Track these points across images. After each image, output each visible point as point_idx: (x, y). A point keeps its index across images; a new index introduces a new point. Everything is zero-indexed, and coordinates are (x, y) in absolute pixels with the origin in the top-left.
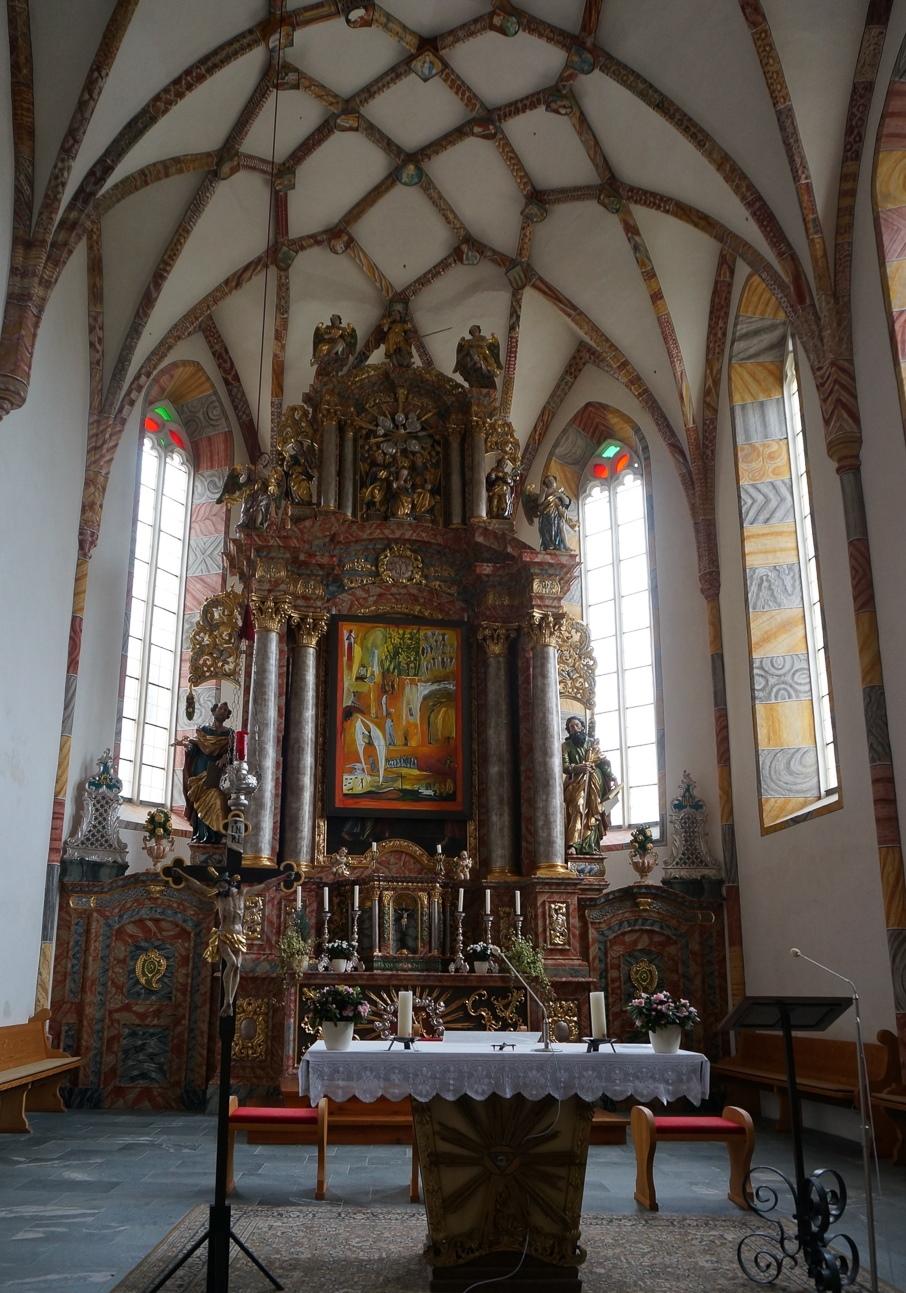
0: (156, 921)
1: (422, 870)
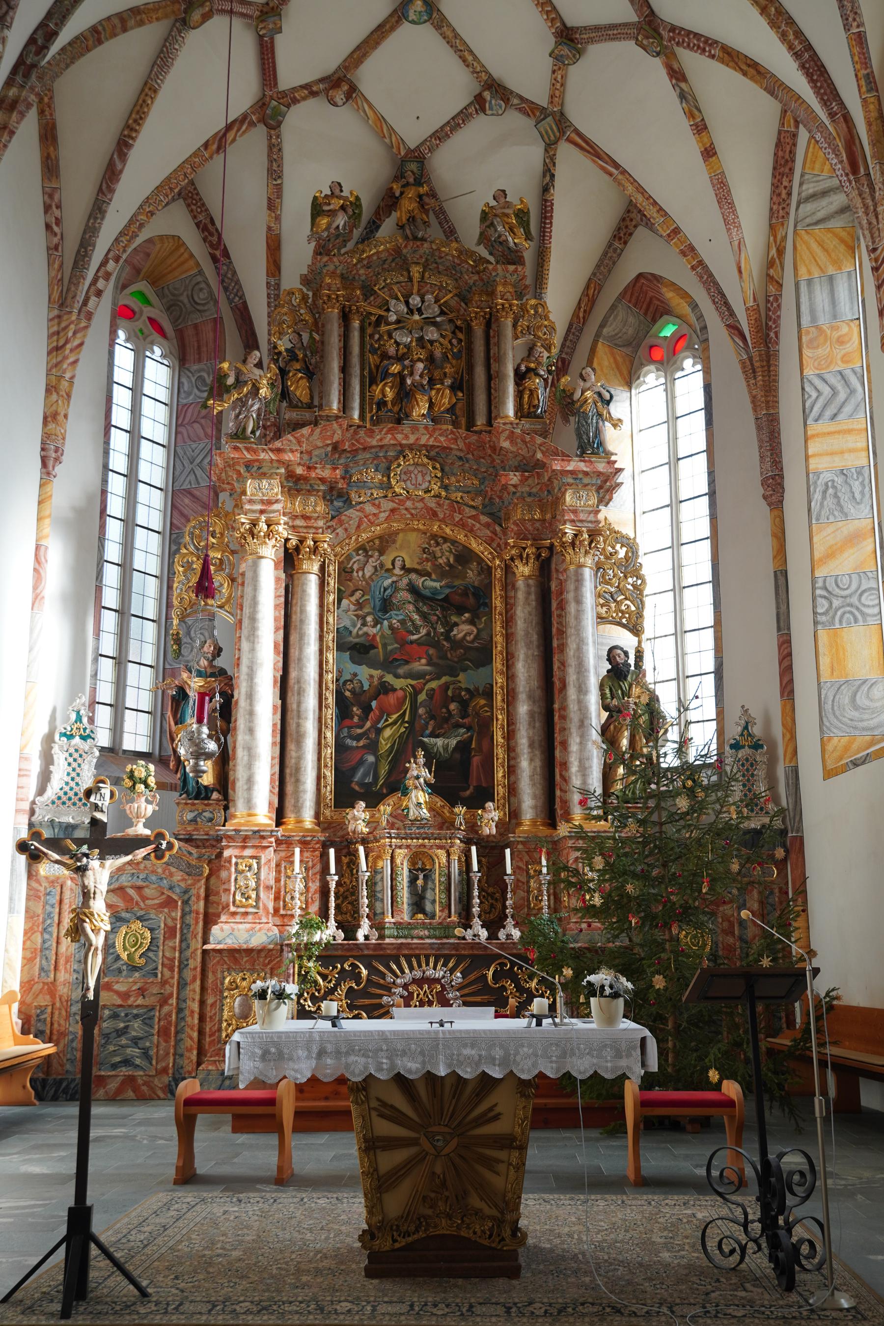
0: (139, 889)
1: (443, 823)
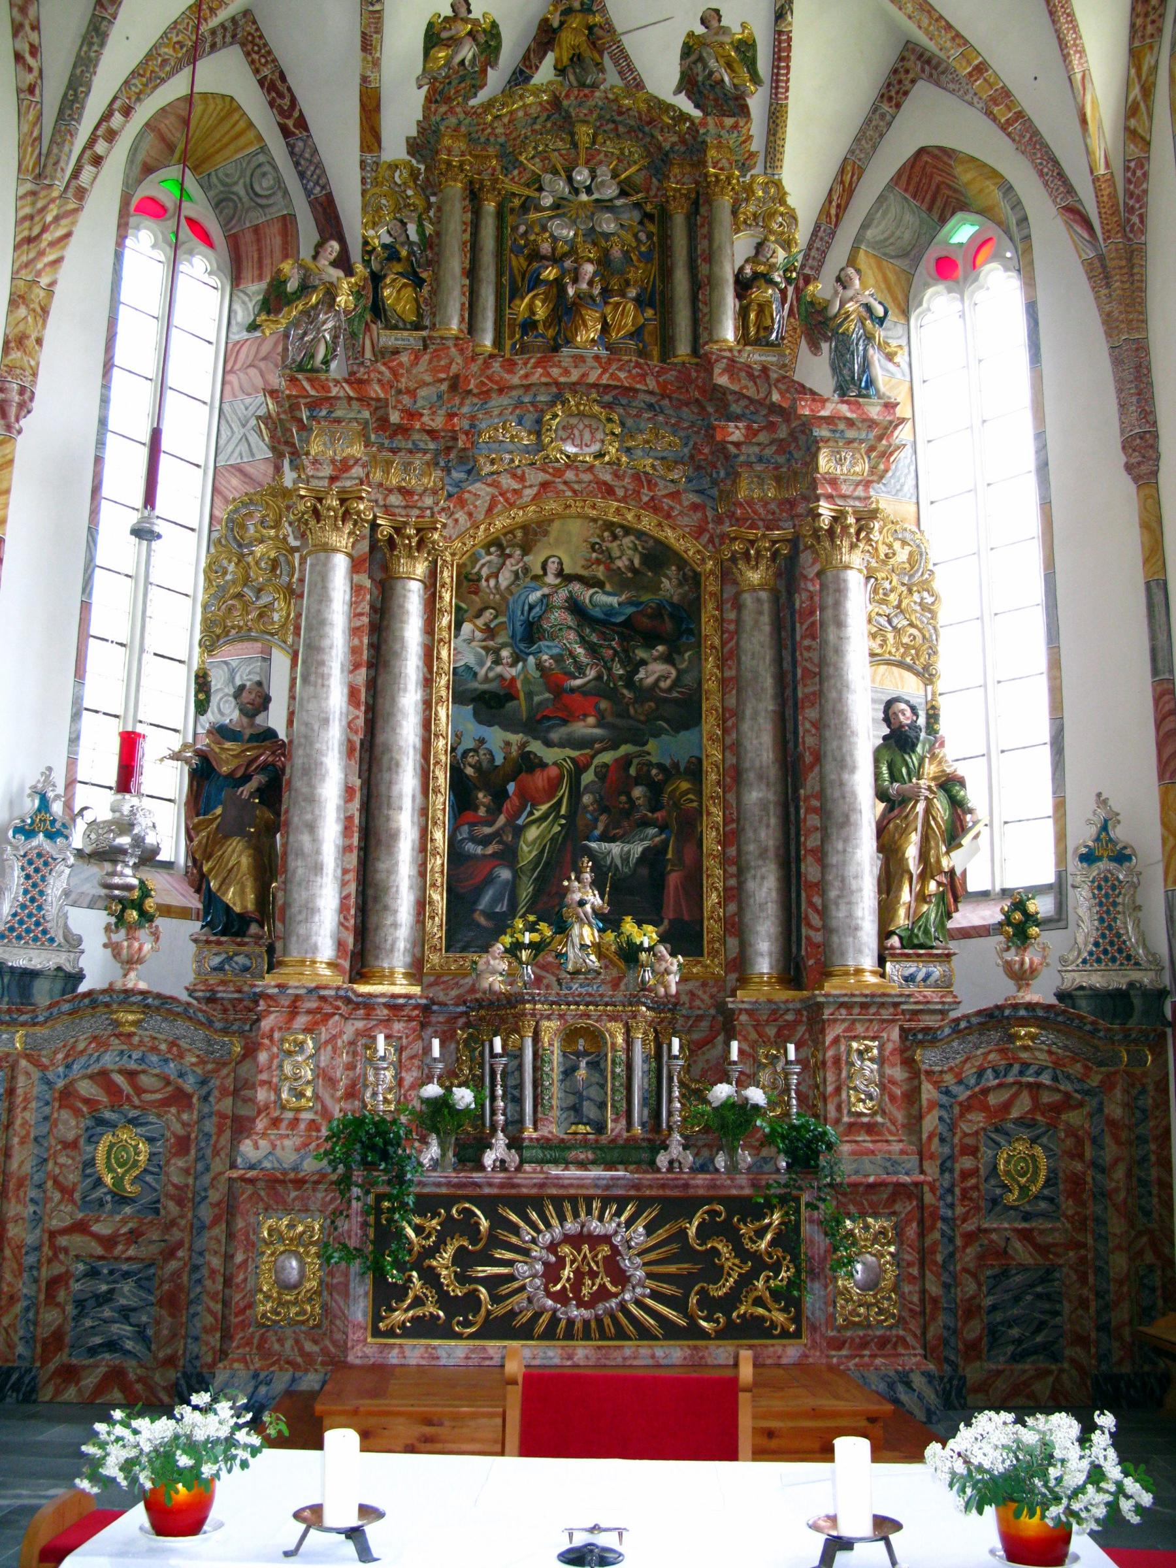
0: (131, 1075)
